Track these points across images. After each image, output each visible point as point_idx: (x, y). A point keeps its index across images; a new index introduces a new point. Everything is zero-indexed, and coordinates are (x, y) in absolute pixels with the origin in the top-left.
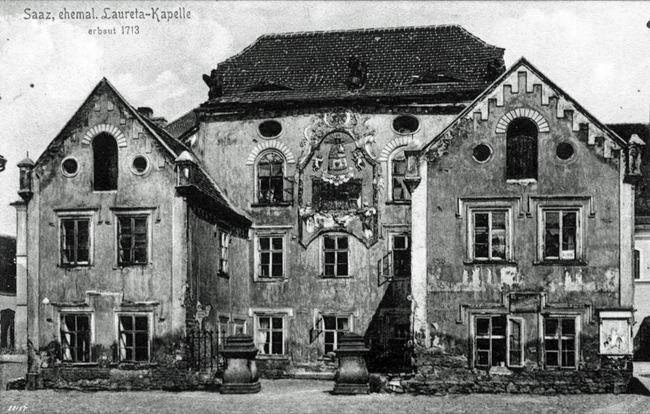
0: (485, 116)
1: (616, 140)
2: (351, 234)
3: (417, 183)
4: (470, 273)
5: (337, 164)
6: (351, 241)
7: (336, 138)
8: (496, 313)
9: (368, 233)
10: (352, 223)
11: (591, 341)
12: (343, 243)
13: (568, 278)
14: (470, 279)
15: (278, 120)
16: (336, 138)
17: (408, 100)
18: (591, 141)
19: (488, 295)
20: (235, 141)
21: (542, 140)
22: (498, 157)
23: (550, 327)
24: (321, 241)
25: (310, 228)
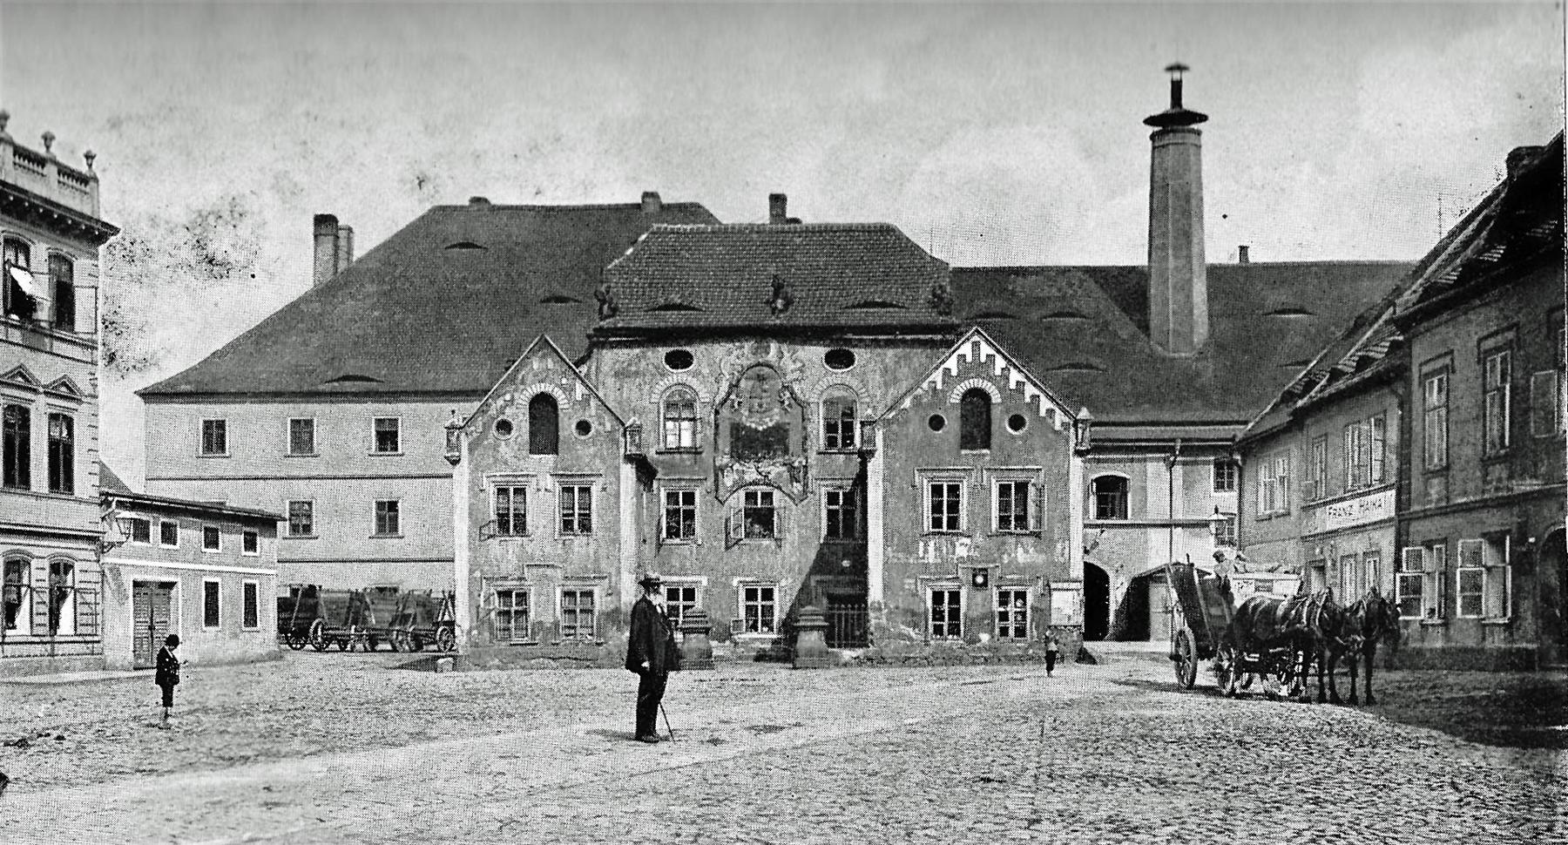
0: (939, 386)
1: (1066, 413)
2: (779, 488)
3: (872, 453)
4: (926, 545)
5: (760, 406)
6: (777, 495)
7: (760, 373)
8: (952, 586)
9: (798, 487)
10: (780, 474)
11: (1042, 612)
12: (767, 497)
13: (1020, 550)
14: (926, 551)
15: (688, 349)
16: (760, 373)
17: (842, 329)
18: (1043, 413)
19: (941, 570)
20: (637, 373)
21: (996, 413)
22: (952, 425)
23: (1004, 598)
24: (742, 493)
25: (728, 480)
